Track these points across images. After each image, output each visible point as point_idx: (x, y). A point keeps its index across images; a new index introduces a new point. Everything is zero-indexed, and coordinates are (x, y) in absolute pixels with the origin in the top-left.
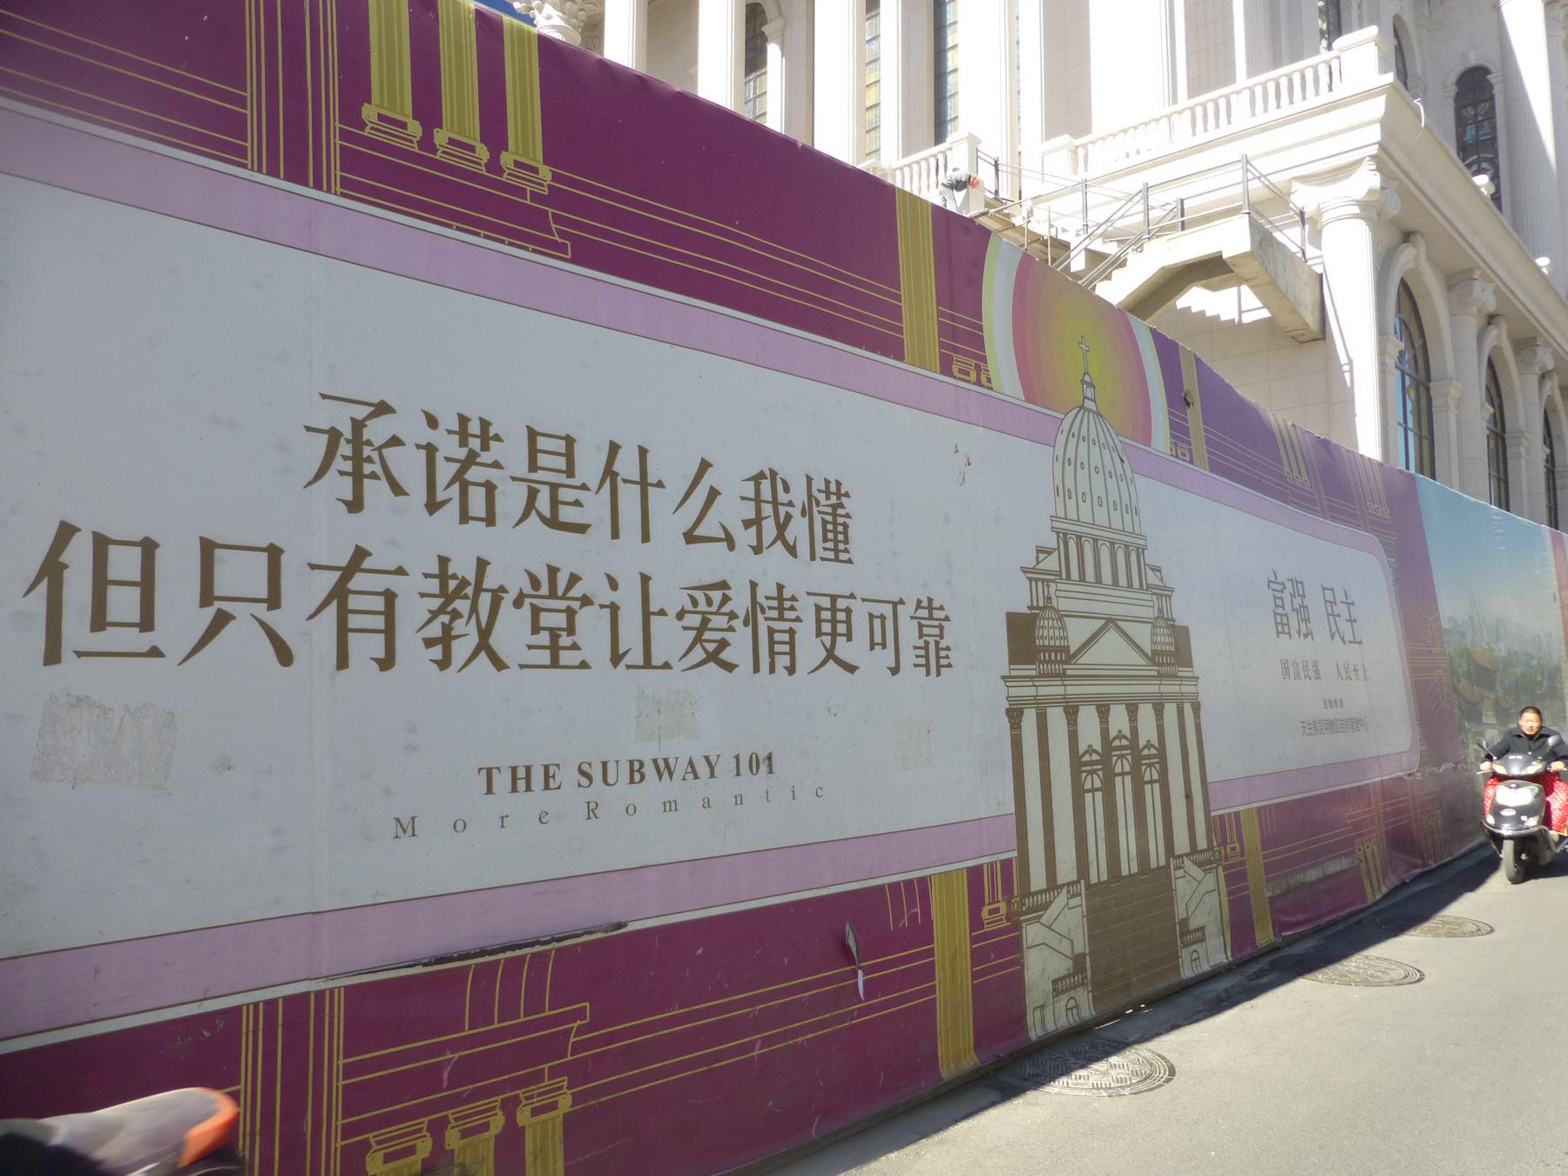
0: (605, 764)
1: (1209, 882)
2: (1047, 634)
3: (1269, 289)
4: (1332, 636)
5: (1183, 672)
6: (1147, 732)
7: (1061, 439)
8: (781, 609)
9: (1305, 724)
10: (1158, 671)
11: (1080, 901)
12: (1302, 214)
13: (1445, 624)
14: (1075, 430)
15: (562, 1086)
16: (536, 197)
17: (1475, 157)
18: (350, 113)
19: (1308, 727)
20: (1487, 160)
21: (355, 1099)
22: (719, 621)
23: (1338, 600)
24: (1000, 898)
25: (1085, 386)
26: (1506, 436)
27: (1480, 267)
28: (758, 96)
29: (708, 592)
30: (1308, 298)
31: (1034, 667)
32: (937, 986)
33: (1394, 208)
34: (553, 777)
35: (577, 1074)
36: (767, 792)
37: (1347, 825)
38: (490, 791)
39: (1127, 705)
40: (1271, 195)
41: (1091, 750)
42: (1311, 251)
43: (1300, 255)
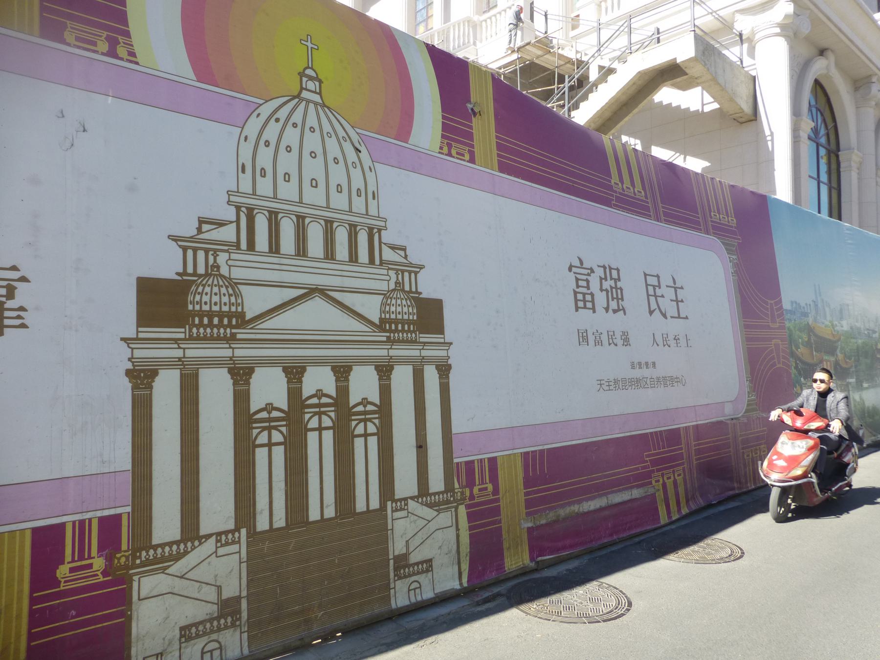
3: (715, 86)
4: (651, 312)
9: (602, 382)
12: (741, 35)
13: (786, 305)
24: (488, 481)
27: (876, 74)
30: (743, 93)
31: (183, 330)
42: (747, 61)
43: (739, 63)
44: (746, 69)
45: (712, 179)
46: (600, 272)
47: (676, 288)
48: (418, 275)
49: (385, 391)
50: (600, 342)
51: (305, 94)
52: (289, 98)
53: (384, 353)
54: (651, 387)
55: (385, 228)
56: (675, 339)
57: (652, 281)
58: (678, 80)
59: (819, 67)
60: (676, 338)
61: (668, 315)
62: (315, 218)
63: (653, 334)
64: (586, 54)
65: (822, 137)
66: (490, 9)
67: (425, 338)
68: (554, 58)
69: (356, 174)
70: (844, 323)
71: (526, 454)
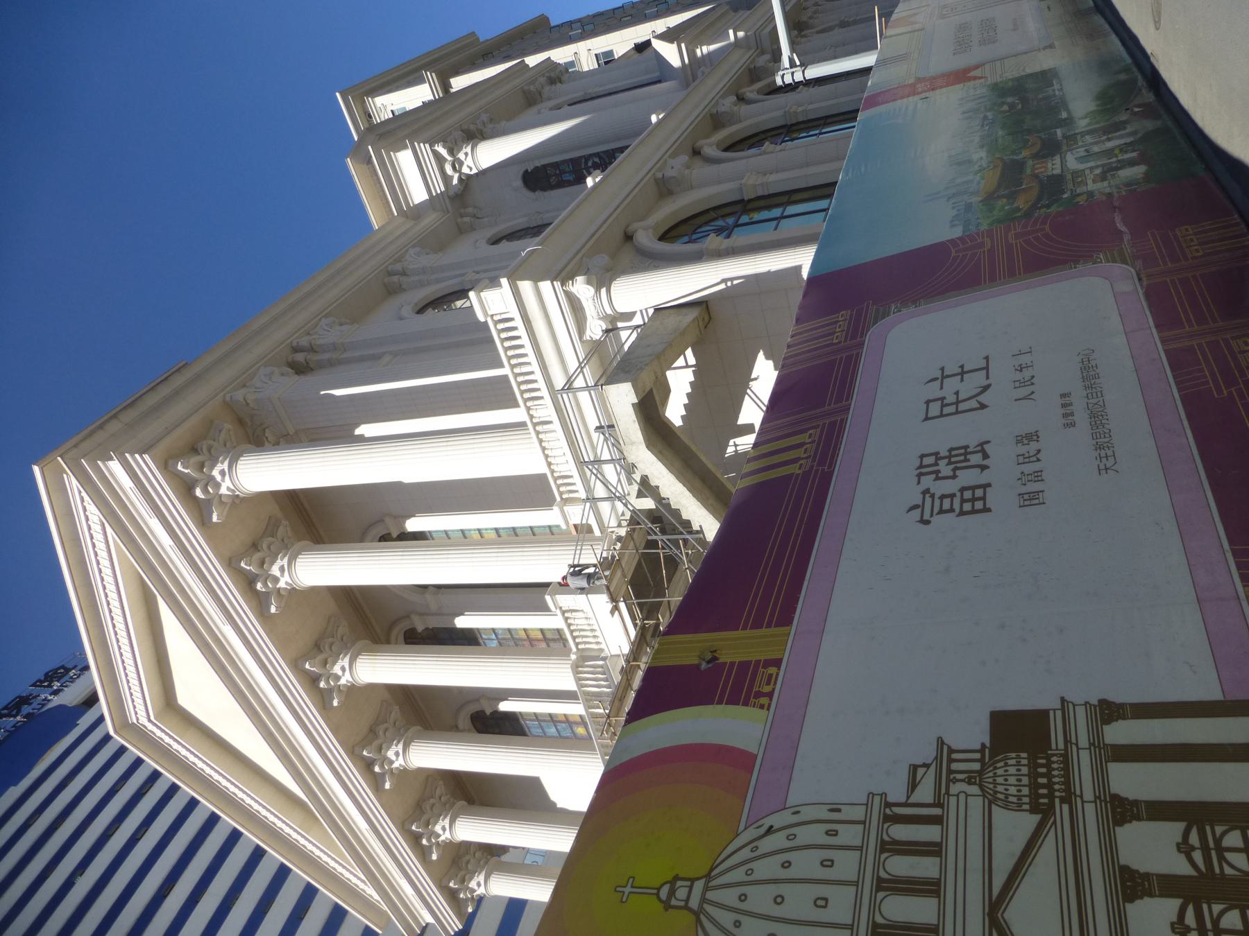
3: (666, 358)
4: (983, 406)
9: (1102, 467)
13: (958, 232)
17: (584, 171)
20: (586, 163)
23: (939, 394)
26: (789, 124)
28: (537, 718)
30: (673, 321)
33: (603, 259)
40: (596, 355)
42: (637, 320)
44: (646, 320)
45: (789, 346)
46: (927, 481)
47: (944, 377)
48: (954, 747)
49: (1160, 811)
50: (1036, 474)
51: (694, 903)
52: (699, 929)
53: (1090, 809)
54: (1102, 396)
55: (884, 795)
56: (1021, 371)
57: (935, 409)
58: (657, 398)
59: (645, 238)
60: (1019, 369)
61: (986, 383)
62: (875, 907)
63: (1016, 400)
64: (623, 514)
65: (727, 223)
66: (563, 640)
67: (1057, 740)
68: (626, 554)
69: (806, 835)
70: (975, 157)
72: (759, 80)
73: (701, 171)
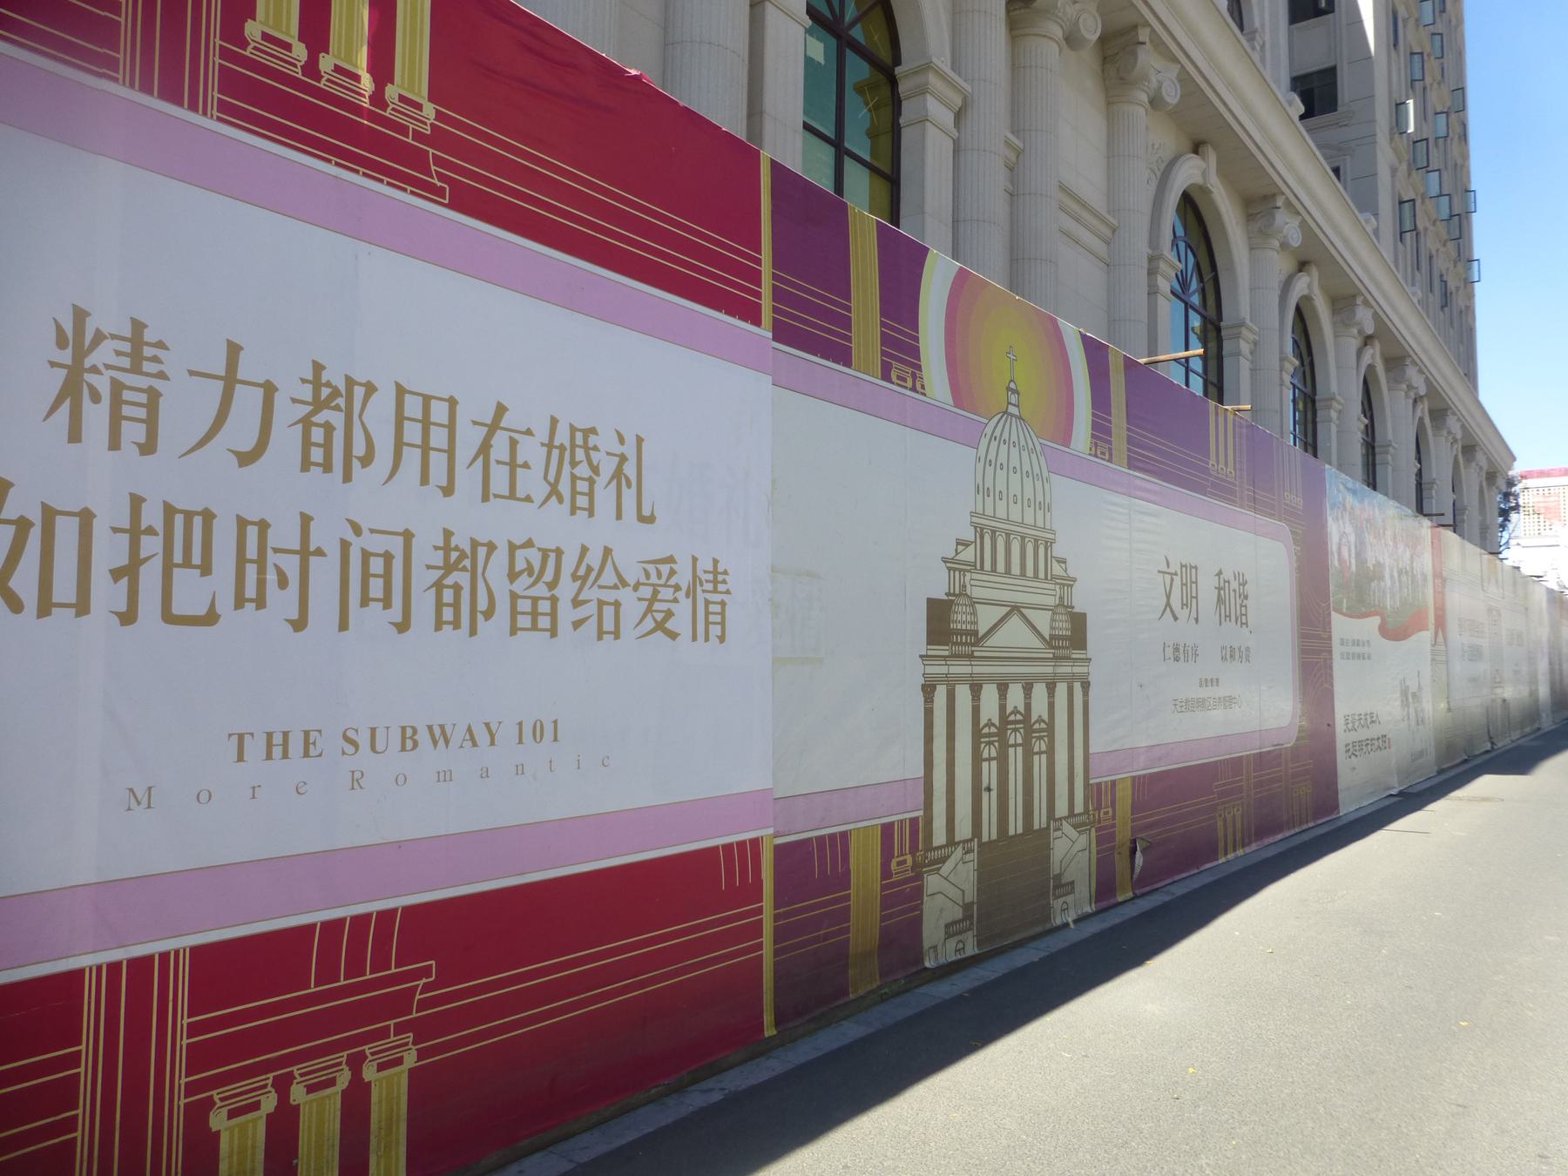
0: (373, 731)
1: (1083, 841)
2: (960, 619)
5: (1076, 654)
6: (1039, 708)
7: (984, 442)
8: (715, 582)
10: (1054, 654)
11: (973, 856)
14: (997, 433)
15: (267, 1084)
16: (418, 136)
18: (233, 32)
19: (1179, 704)
21: (199, 1058)
22: (666, 593)
24: (908, 852)
25: (1010, 393)
26: (1317, 397)
29: (658, 566)
32: (764, 955)
34: (314, 743)
35: (421, 1030)
36: (551, 762)
37: (1214, 793)
38: (240, 758)
39: (971, 686)
41: (1040, 720)
71: (1134, 778)
72: (1388, 370)
73: (1279, 265)
